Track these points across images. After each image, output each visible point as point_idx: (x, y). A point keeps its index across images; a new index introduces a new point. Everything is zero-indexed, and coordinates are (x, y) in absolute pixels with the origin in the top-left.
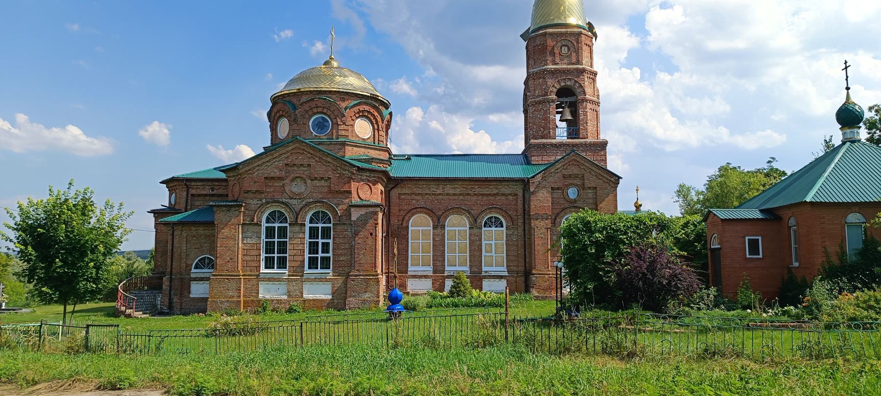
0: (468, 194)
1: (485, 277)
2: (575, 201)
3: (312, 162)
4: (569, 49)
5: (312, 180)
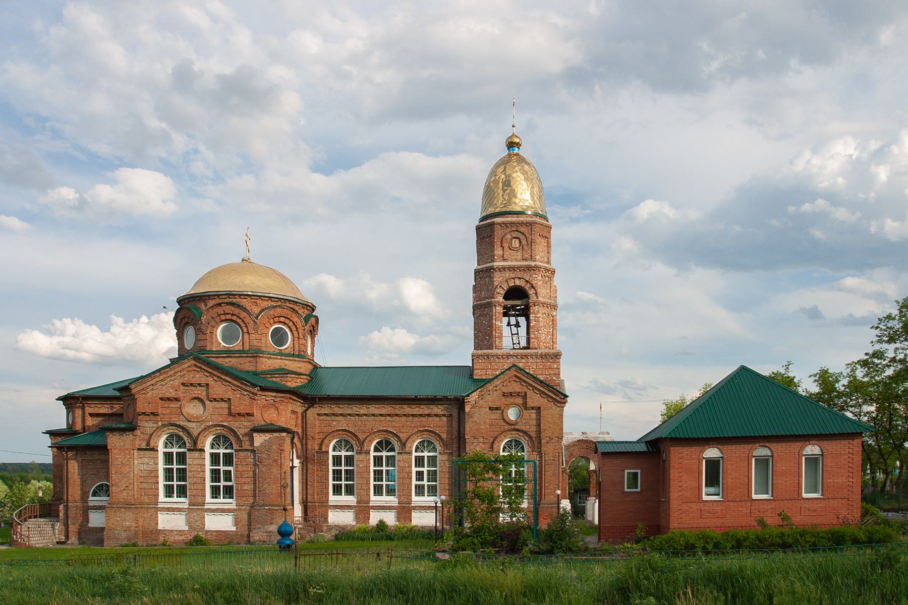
0: (397, 415)
1: (415, 508)
2: (516, 423)
4: (520, 242)
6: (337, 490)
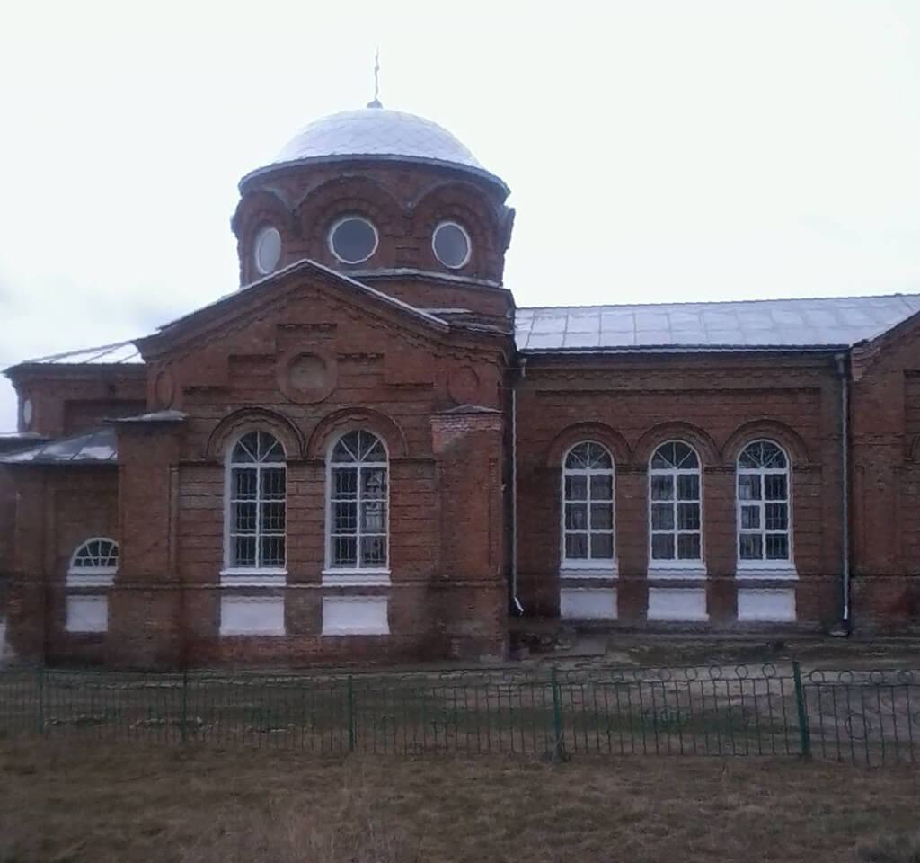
3: (340, 319)
5: (340, 361)
6: (244, 553)
